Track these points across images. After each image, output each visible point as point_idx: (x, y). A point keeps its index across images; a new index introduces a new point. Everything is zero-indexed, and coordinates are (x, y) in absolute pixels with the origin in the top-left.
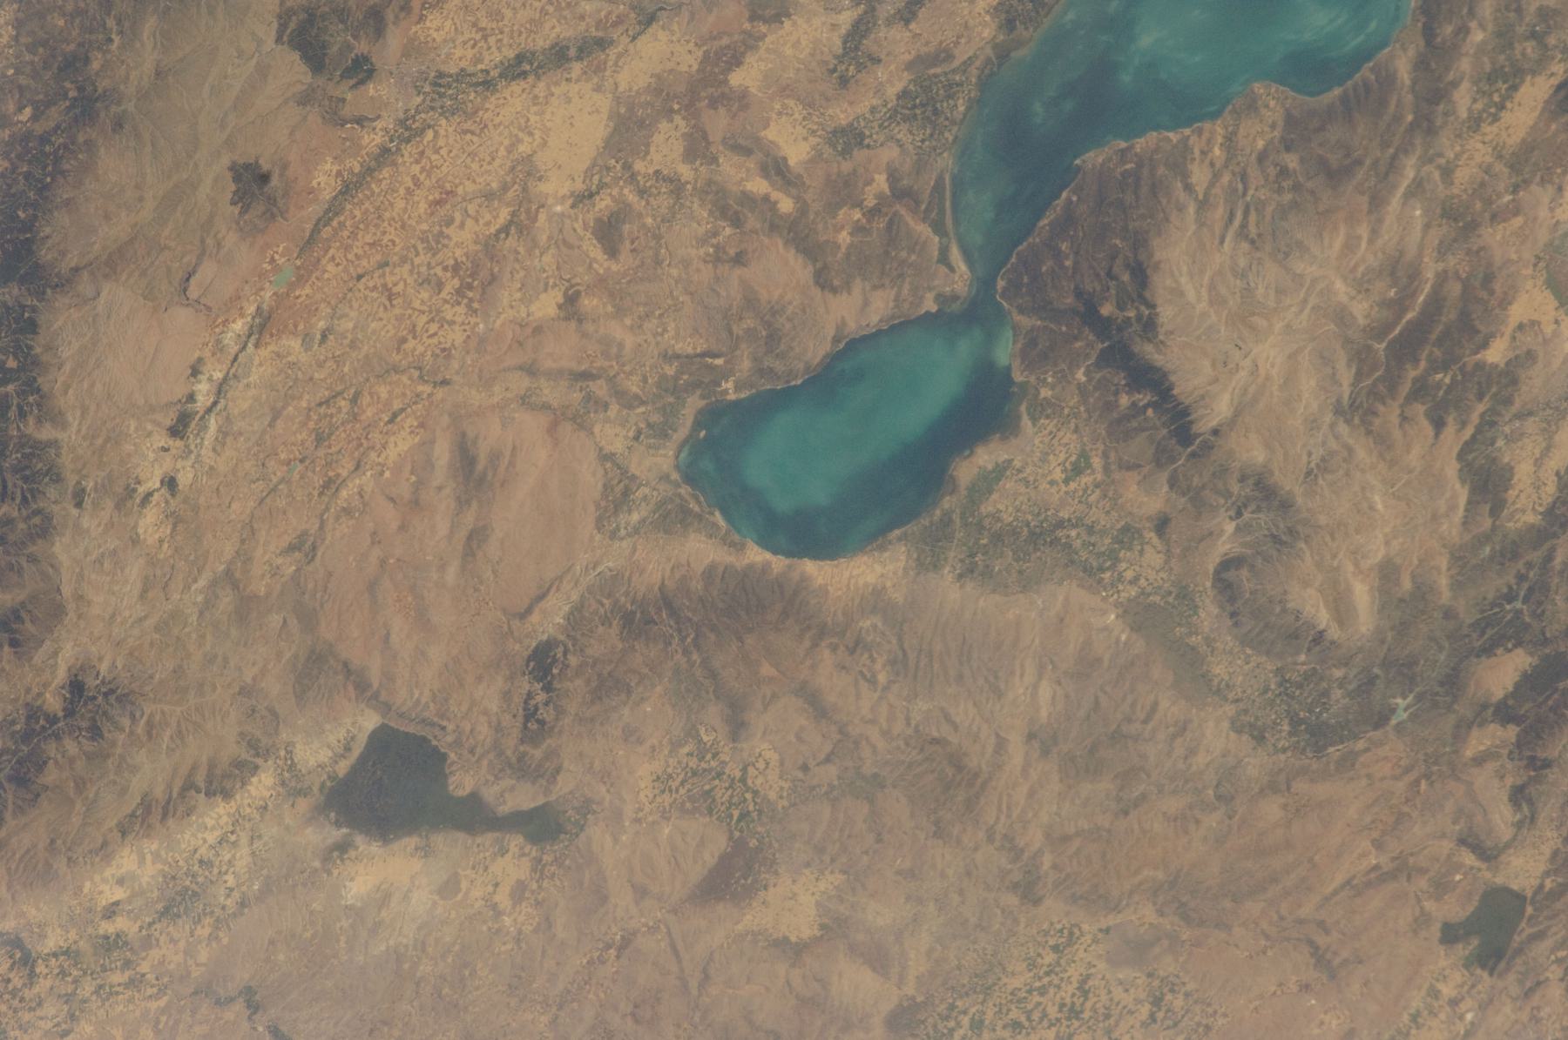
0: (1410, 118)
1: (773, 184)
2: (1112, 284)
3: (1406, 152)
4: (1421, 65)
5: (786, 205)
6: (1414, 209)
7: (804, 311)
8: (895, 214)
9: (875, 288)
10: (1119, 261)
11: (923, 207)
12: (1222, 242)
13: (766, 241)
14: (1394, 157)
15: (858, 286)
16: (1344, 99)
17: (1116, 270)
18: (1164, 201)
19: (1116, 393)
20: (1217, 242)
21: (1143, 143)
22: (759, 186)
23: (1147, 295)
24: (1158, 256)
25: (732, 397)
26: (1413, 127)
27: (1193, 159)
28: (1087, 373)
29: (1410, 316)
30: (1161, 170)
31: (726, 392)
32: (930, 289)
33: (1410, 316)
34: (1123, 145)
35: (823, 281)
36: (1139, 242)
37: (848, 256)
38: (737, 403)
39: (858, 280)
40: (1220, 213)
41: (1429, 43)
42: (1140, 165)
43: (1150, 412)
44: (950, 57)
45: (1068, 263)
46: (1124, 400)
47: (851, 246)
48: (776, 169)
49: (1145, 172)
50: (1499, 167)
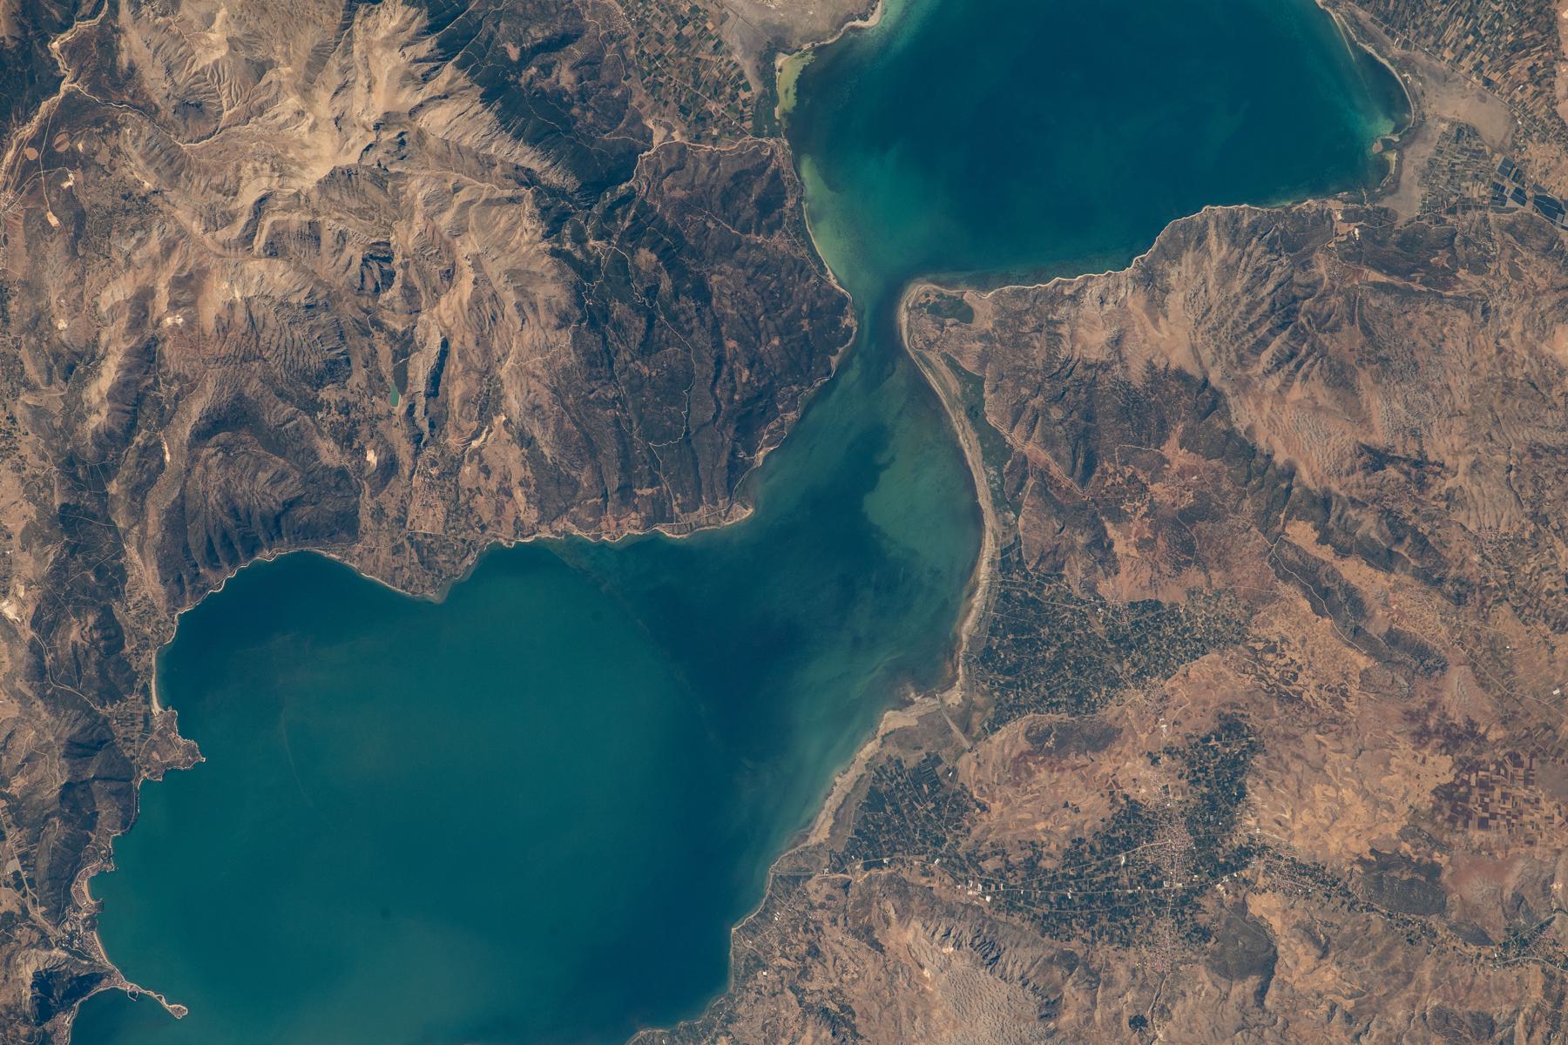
0: (113, 488)
1: (1334, 575)
3: (110, 434)
4: (114, 579)
5: (1302, 533)
6: (71, 330)
7: (1241, 358)
8: (1083, 482)
9: (1105, 367)
11: (1030, 482)
13: (1335, 487)
14: (131, 429)
15: (1136, 373)
16: (253, 547)
17: (640, 323)
18: (568, 425)
19: (583, 95)
20: (454, 345)
22: (1354, 571)
23: (571, 275)
24: (565, 339)
25: (1336, 207)
26: (105, 471)
27: (523, 483)
28: (647, 137)
29: (28, 131)
30: (585, 477)
31: (1350, 217)
32: (985, 337)
33: (28, 131)
34: (665, 531)
35: (1209, 402)
36: (598, 361)
37: (1163, 426)
38: (1319, 188)
39: (1137, 383)
40: (457, 390)
41: (107, 613)
42: (626, 491)
43: (514, 54)
44: (1037, 737)
46: (565, 77)
47: (1162, 439)
48: (1328, 597)
49: (614, 482)
50: (836, 893)
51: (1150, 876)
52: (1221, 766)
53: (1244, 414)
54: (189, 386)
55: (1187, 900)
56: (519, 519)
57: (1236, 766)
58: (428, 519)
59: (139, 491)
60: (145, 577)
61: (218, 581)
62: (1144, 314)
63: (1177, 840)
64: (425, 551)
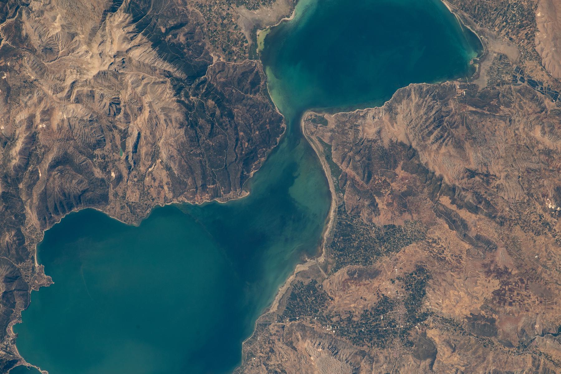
0: (21, 186)
1: (457, 215)
2: (209, 118)
3: (20, 167)
5: (445, 200)
6: (6, 129)
7: (423, 138)
8: (367, 182)
9: (375, 141)
10: (207, 131)
12: (139, 134)
13: (457, 184)
14: (27, 165)
15: (386, 143)
16: (71, 208)
17: (209, 126)
18: (183, 163)
19: (188, 45)
21: (203, 199)
22: (464, 214)
24: (182, 132)
25: (457, 84)
26: (18, 180)
27: (167, 184)
28: (211, 59)
30: (189, 181)
31: (462, 87)
32: (332, 131)
34: (218, 200)
35: (412, 154)
36: (194, 140)
38: (451, 77)
39: (386, 147)
40: (143, 150)
41: (19, 230)
42: (204, 186)
43: (163, 30)
44: (351, 274)
45: (241, 134)
46: (182, 39)
47: (395, 167)
48: (455, 223)
49: (200, 183)
51: (391, 323)
52: (417, 284)
53: (424, 158)
54: (48, 149)
55: (405, 332)
56: (166, 196)
57: (422, 284)
58: (133, 197)
59: (30, 187)
60: (32, 218)
61: (59, 219)
62: (389, 122)
63: (401, 310)
64: (132, 208)
